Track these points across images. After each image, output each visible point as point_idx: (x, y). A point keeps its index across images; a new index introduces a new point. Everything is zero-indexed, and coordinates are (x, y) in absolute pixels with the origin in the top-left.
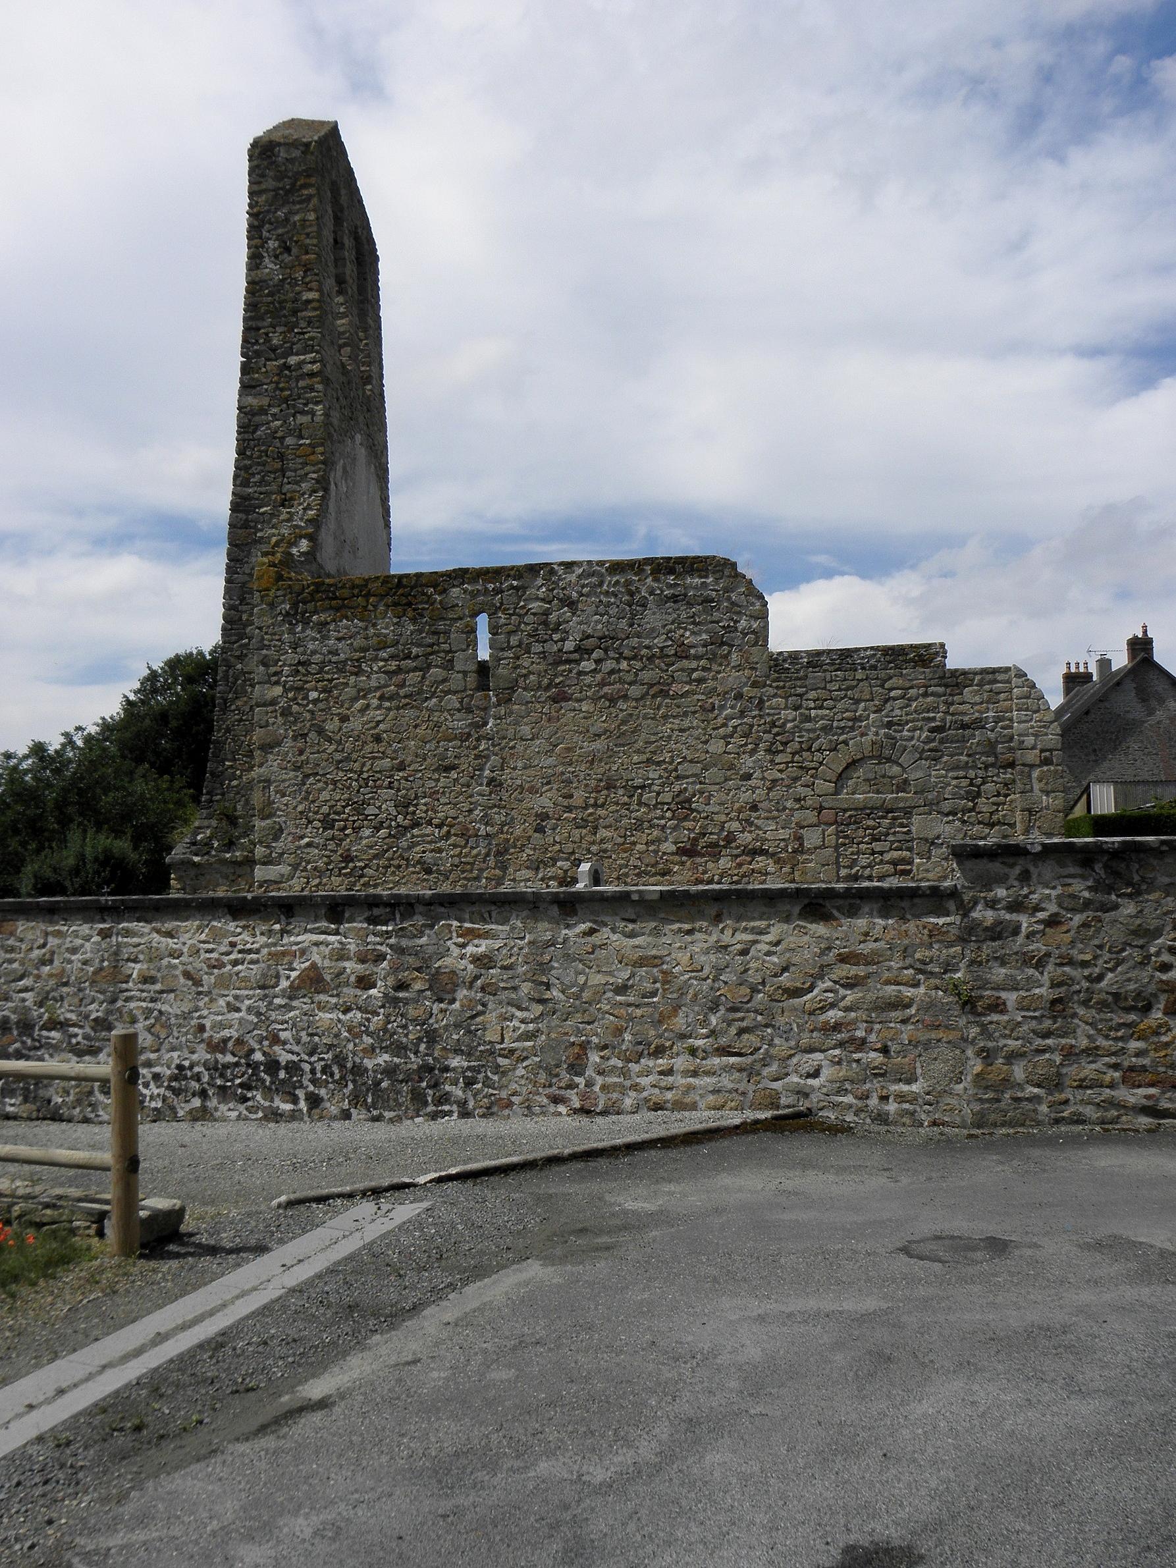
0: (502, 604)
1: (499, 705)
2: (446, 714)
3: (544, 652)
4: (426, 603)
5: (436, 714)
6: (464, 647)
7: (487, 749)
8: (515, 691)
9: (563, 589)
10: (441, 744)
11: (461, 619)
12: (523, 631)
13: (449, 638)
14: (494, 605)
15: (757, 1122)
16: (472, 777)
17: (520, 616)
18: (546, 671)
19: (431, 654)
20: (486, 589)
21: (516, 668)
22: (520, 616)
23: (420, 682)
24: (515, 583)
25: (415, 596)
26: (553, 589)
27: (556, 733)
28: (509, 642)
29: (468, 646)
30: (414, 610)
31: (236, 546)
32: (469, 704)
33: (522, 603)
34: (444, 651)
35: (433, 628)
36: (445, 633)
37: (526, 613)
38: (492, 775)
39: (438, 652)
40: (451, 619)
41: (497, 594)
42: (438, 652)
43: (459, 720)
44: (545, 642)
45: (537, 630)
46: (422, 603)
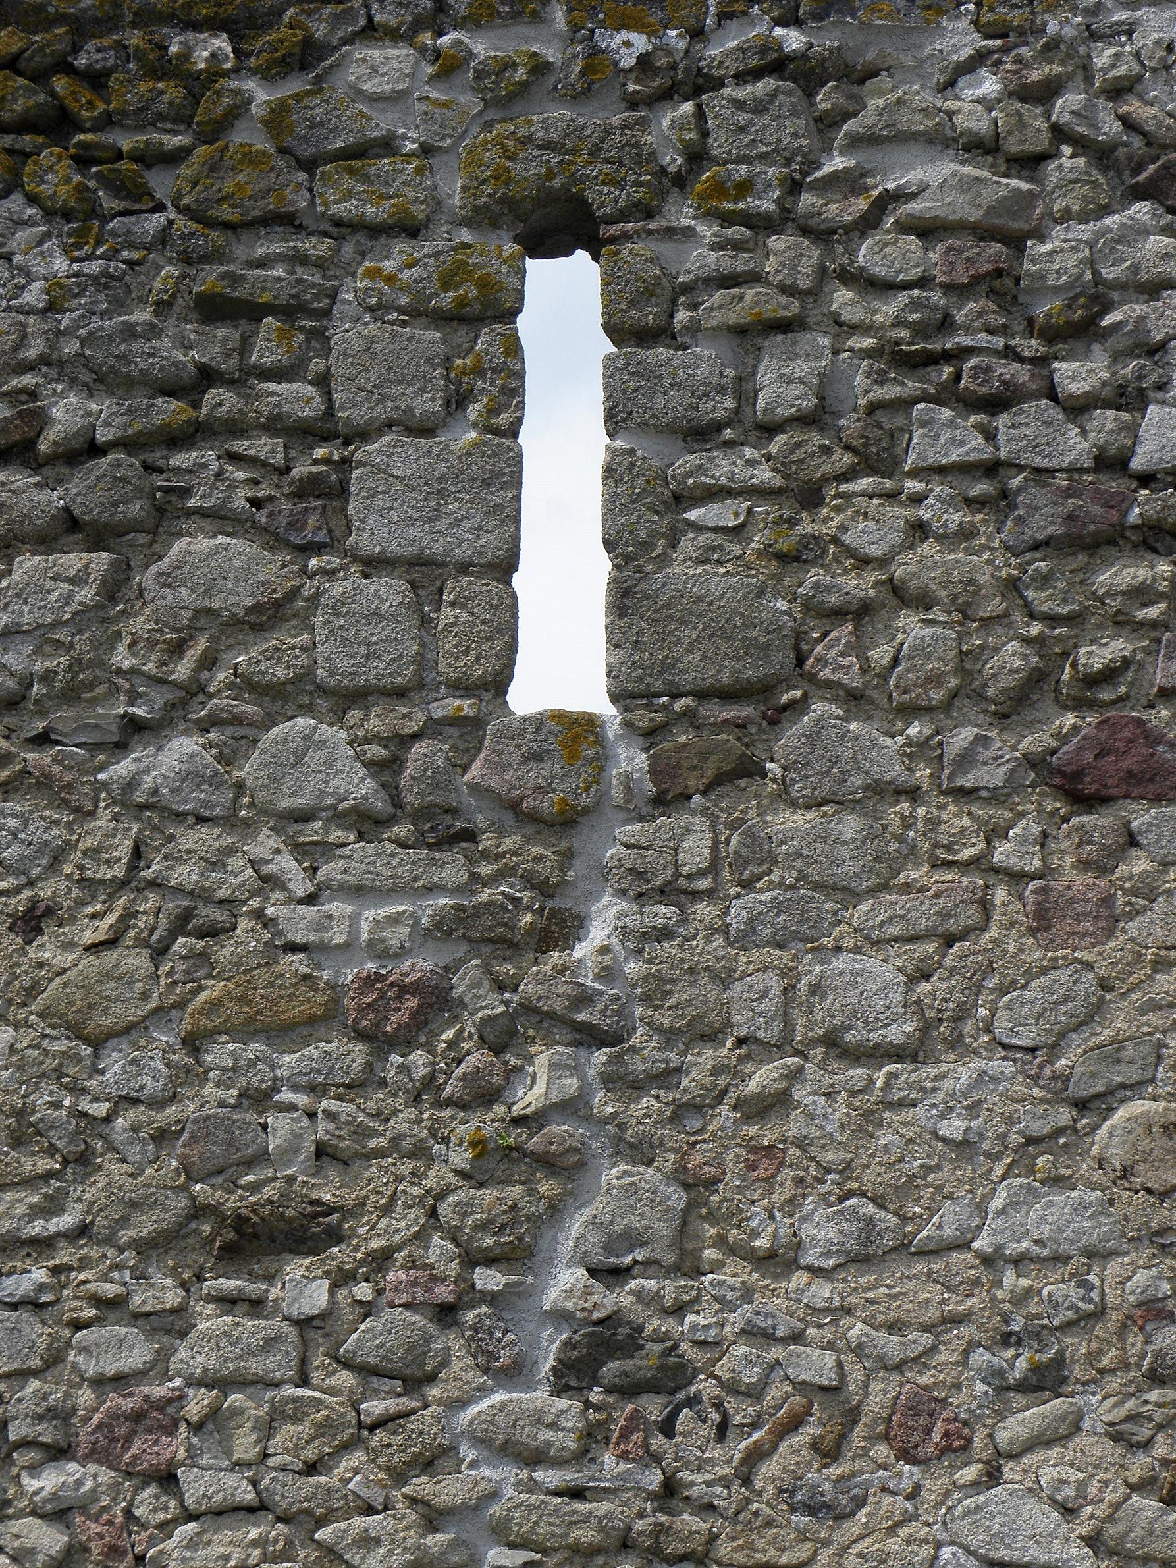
0: (697, 157)
1: (663, 802)
2: (265, 843)
3: (992, 469)
4: (181, 118)
5: (190, 838)
6: (427, 404)
7: (573, 1107)
8: (778, 717)
9: (1118, 91)
10: (218, 1054)
11: (411, 230)
12: (842, 327)
13: (320, 336)
14: (645, 158)
15: (848, 480)
16: (446, 1314)
17: (822, 234)
18: (1012, 586)
19: (177, 439)
20: (597, 60)
21: (790, 559)
22: (822, 234)
23: (80, 620)
24: (793, 40)
25: (96, 80)
26: (1046, 93)
27: (1095, 1013)
28: (744, 389)
29: (458, 401)
30: (83, 161)
31: (616, 646)
32: (436, 780)
33: (838, 162)
34: (275, 425)
35: (209, 278)
36: (290, 311)
37: (868, 223)
38: (608, 1300)
39: (235, 428)
40: (343, 227)
41: (667, 95)
42: (235, 428)
43: (358, 892)
44: (995, 404)
45: (945, 324)
46: (145, 117)
